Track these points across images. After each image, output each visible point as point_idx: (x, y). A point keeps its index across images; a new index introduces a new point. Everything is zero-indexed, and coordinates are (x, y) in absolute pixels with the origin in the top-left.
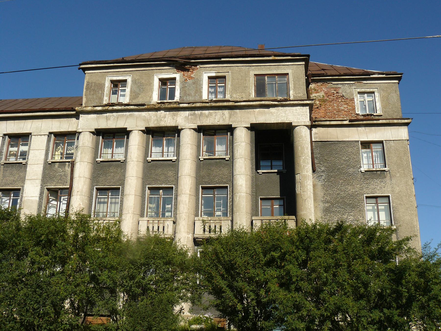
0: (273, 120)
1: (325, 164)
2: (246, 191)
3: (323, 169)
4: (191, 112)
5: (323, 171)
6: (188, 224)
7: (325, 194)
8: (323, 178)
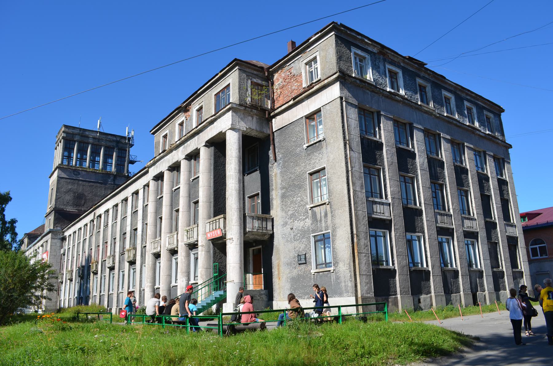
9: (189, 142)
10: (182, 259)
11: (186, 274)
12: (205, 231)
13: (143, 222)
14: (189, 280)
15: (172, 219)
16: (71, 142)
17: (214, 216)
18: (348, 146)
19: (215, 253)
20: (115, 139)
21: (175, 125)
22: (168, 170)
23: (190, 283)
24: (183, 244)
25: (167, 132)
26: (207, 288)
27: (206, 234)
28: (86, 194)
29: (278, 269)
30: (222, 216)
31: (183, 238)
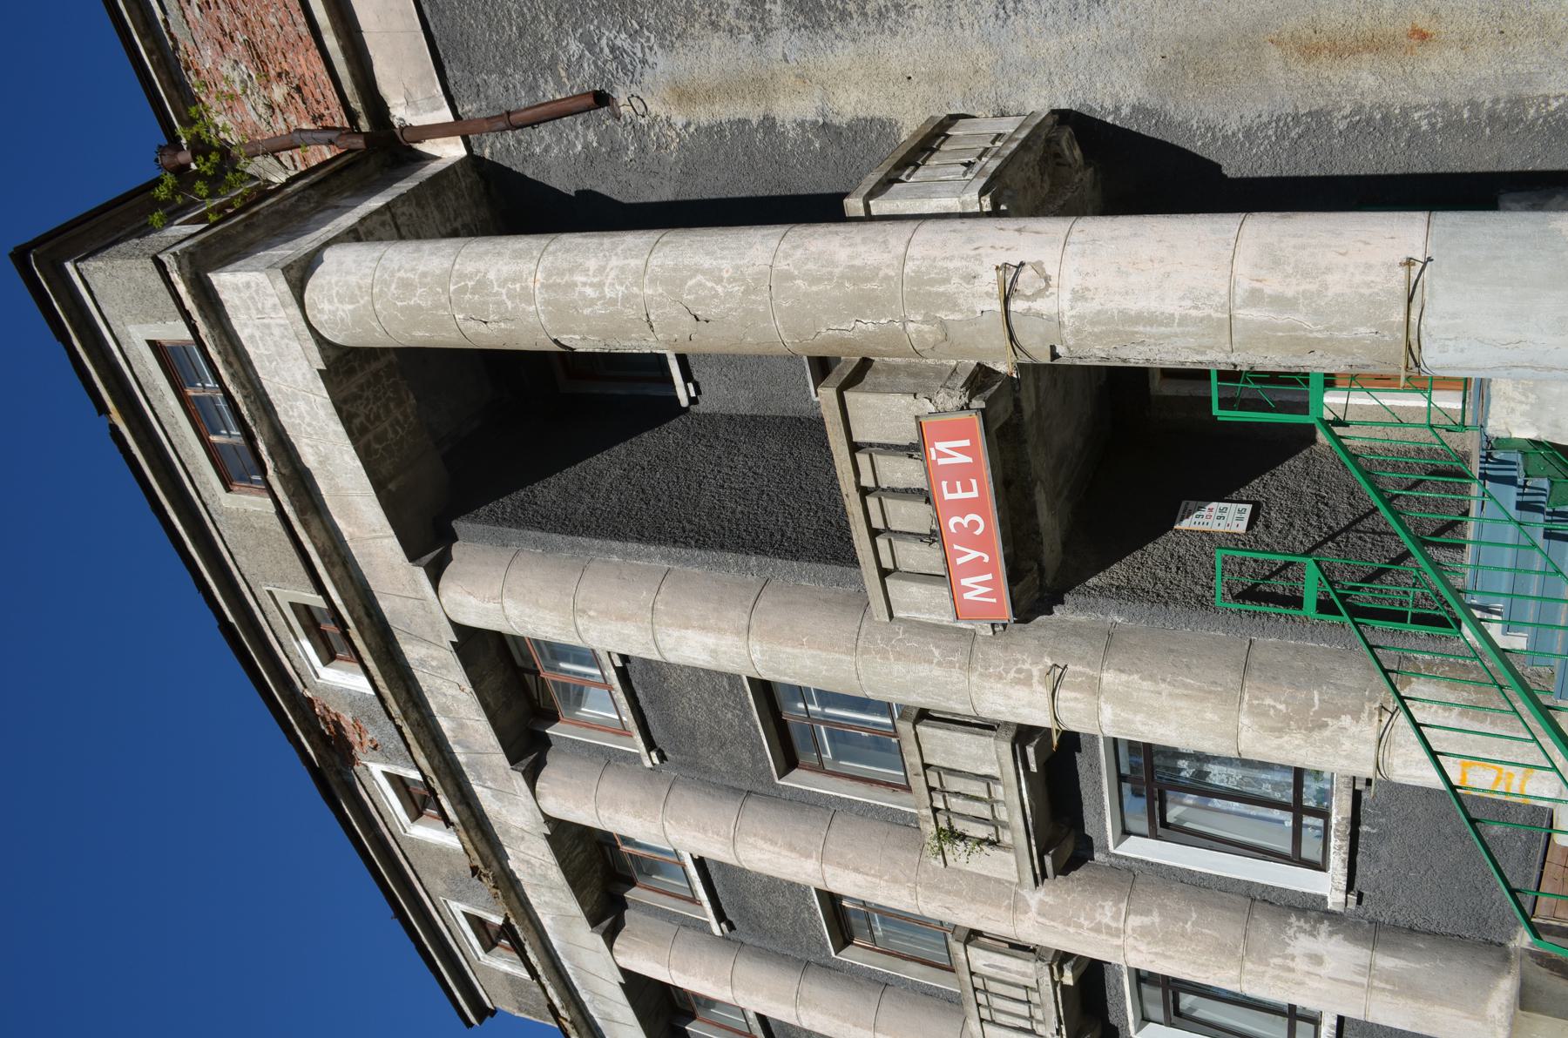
0: (347, 458)
1: (547, 32)
2: (738, 634)
3: (575, 47)
4: (471, 779)
5: (591, 46)
6: (973, 900)
7: (715, 25)
8: (622, 40)
9: (445, 724)
10: (1144, 932)
11: (1265, 927)
12: (937, 642)
14: (1310, 909)
15: (884, 984)
17: (854, 562)
19: (1129, 593)
22: (610, 937)
23: (1336, 898)
24: (1036, 897)
26: (1416, 688)
27: (954, 638)
29: (1343, 49)
31: (984, 888)
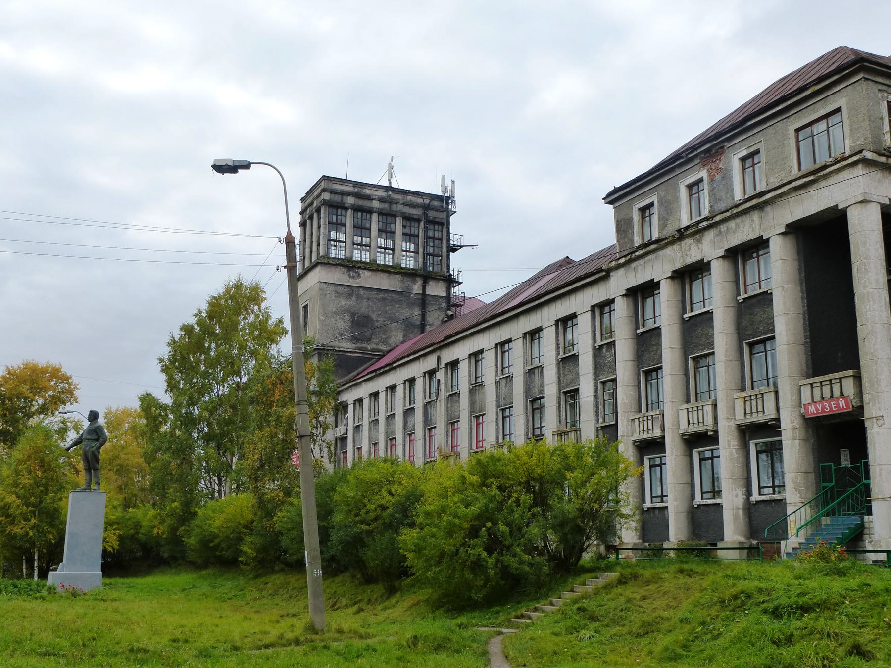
13: (596, 379)
14: (749, 493)
16: (339, 211)
18: (812, 177)
20: (420, 201)
21: (676, 189)
25: (654, 199)
28: (374, 316)
30: (850, 372)
